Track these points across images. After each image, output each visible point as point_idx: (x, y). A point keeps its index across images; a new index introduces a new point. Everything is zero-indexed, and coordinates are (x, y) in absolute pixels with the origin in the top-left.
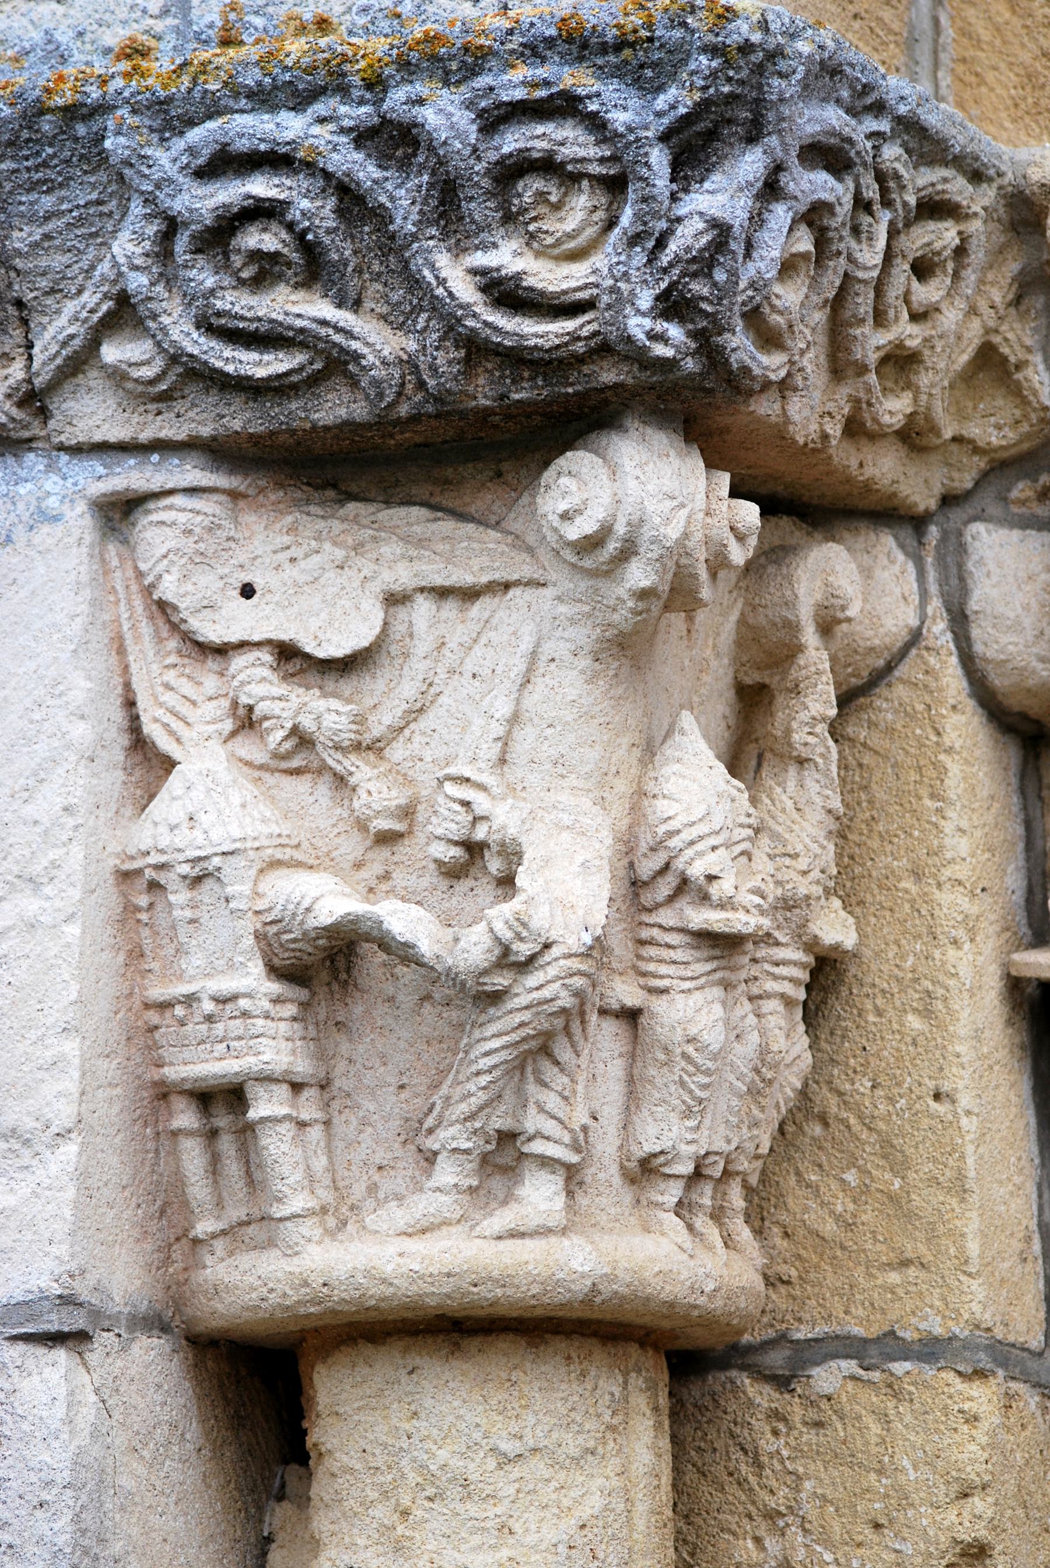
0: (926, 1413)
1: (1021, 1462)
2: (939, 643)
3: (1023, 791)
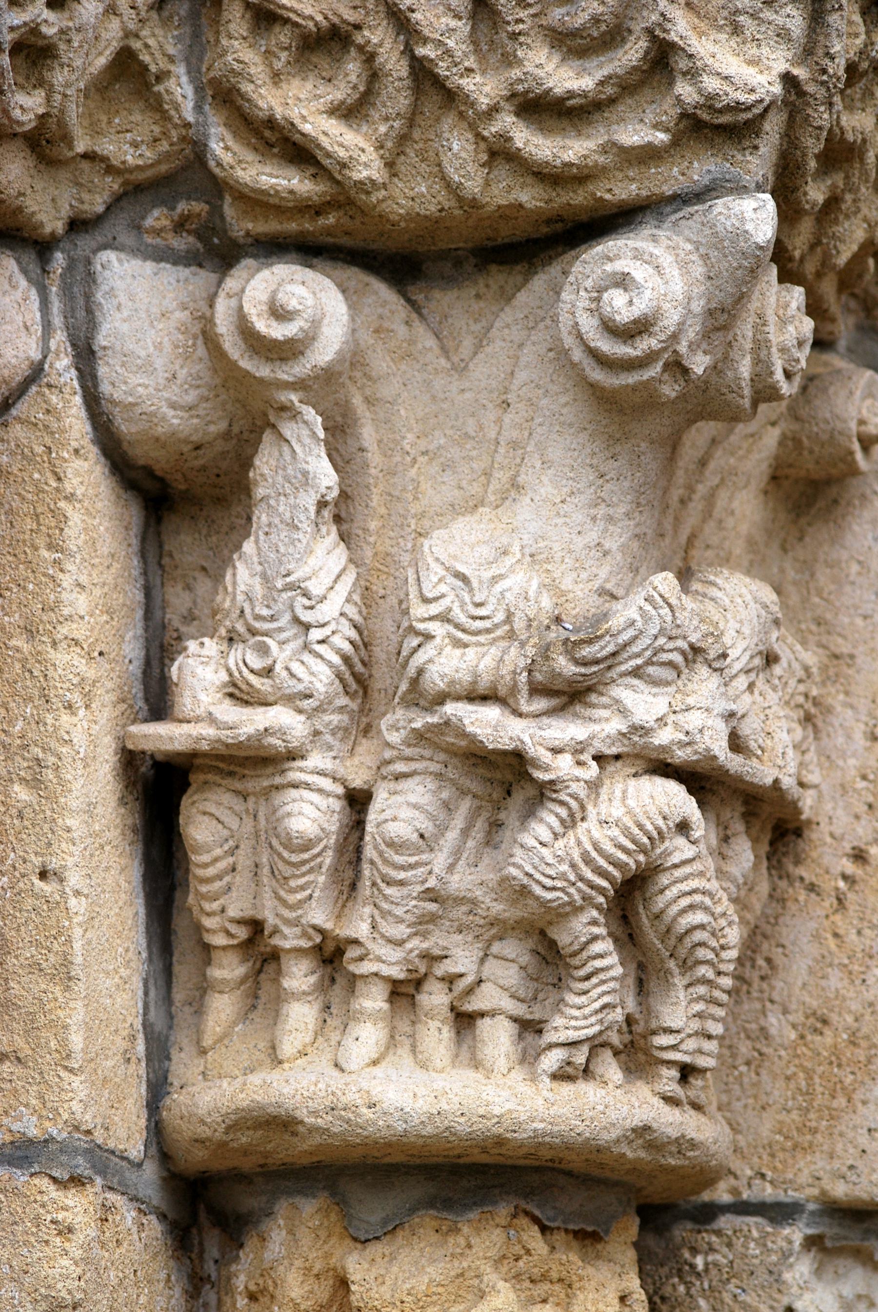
0: (15, 1223)
1: (114, 1281)
2: (62, 380)
3: (143, 554)
